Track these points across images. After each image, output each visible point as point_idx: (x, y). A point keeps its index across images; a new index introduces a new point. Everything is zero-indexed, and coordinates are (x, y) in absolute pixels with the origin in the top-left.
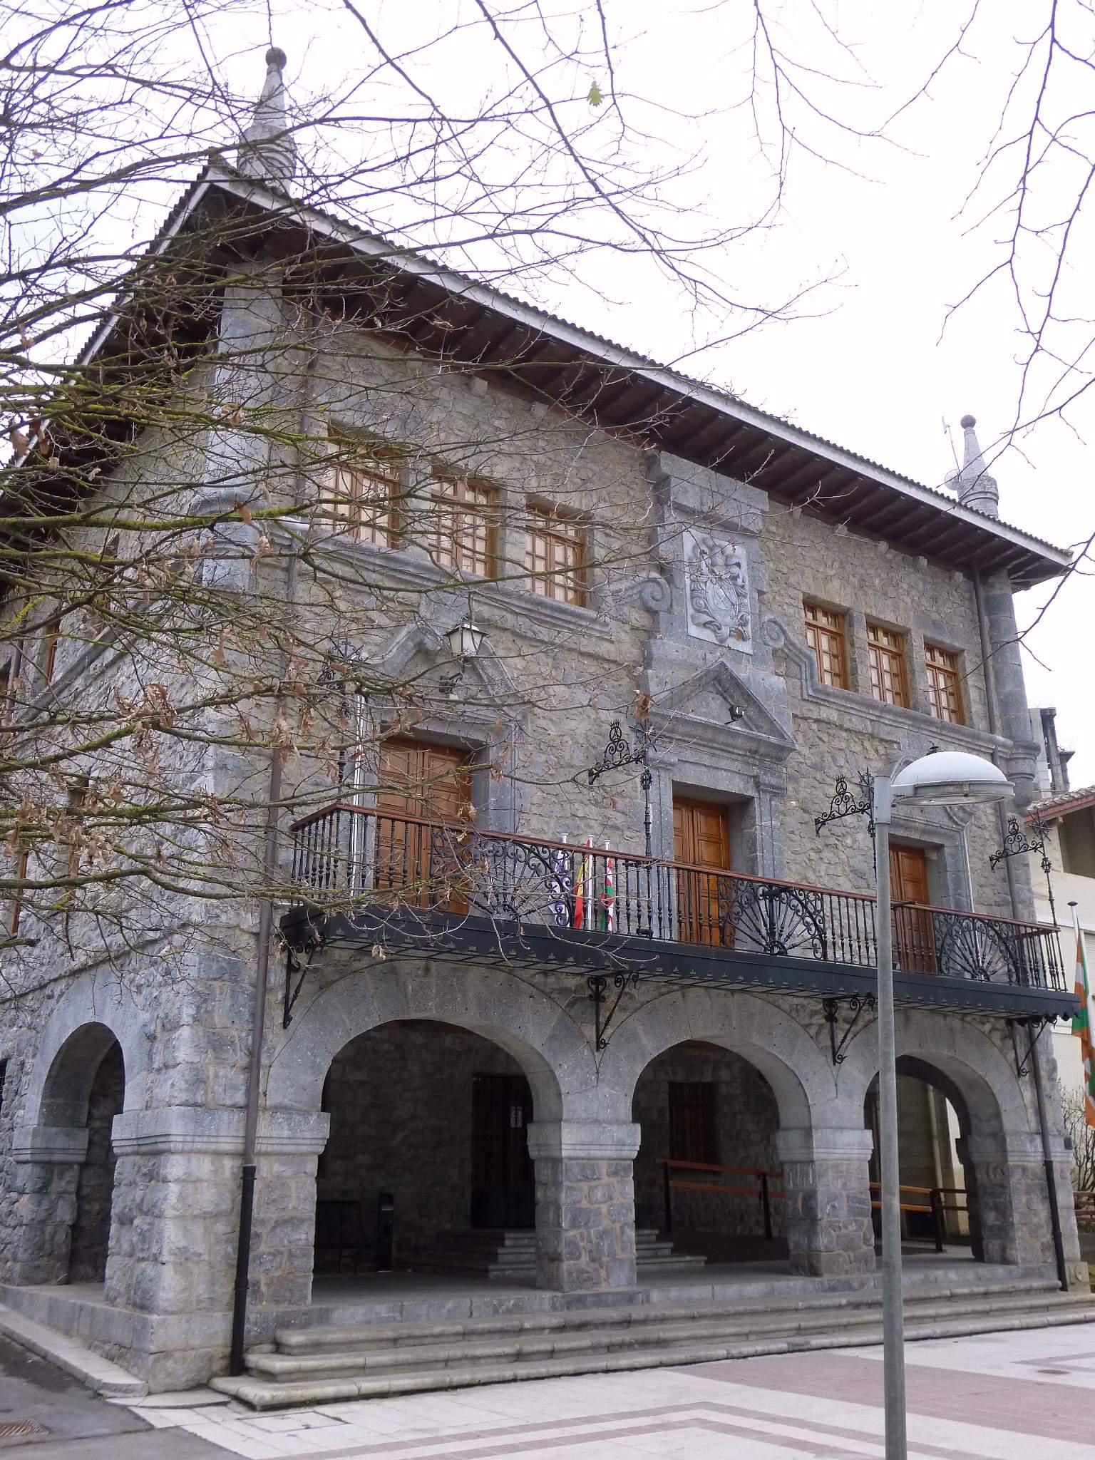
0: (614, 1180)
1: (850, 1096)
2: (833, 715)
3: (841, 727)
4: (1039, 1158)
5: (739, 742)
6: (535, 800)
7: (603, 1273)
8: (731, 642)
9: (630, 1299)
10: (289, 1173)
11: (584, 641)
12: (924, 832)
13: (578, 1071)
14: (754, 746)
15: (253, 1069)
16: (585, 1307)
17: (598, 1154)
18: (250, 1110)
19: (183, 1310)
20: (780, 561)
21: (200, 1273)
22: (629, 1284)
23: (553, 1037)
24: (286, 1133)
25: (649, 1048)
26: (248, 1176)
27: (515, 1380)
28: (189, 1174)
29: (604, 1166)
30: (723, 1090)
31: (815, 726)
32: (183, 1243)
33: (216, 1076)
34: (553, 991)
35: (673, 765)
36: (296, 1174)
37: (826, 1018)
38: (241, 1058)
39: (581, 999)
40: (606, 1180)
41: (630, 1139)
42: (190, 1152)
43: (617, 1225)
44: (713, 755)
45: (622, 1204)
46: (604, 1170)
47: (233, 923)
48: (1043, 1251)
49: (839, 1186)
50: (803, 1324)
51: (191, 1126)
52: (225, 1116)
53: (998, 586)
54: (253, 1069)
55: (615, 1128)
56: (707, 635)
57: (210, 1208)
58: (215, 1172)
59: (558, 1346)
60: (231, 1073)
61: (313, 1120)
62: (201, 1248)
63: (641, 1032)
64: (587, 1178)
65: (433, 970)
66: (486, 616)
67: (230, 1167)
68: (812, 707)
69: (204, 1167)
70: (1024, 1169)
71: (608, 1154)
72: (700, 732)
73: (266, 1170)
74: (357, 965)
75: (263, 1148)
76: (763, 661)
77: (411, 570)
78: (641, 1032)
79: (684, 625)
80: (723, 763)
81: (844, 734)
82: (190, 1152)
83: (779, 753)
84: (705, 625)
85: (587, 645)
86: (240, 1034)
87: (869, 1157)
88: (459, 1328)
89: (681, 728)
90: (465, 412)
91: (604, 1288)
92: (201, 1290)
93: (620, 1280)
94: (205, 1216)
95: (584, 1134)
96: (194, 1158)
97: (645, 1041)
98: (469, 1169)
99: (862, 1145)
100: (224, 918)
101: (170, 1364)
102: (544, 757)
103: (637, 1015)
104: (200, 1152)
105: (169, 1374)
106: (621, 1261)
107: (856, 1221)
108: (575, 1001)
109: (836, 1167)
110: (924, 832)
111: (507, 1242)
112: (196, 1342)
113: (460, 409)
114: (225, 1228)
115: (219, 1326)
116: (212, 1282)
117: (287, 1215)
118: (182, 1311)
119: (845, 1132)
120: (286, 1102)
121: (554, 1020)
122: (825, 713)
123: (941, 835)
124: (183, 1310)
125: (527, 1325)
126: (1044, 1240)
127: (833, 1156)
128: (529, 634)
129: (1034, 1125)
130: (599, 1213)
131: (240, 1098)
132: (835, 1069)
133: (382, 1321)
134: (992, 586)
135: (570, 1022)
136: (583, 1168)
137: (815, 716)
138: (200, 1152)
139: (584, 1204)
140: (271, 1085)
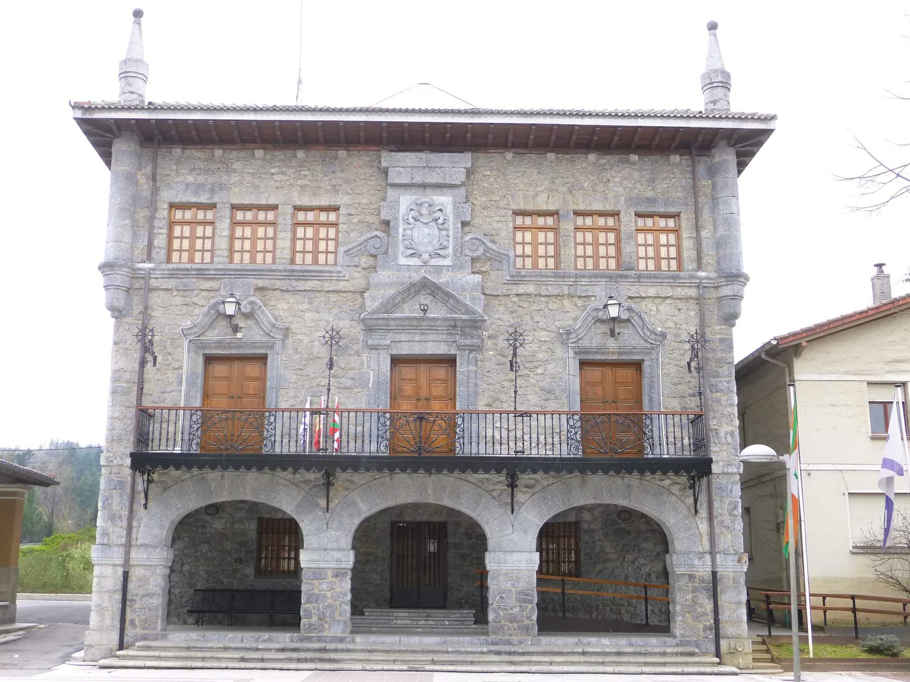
0: (335, 579)
1: (525, 532)
2: (531, 289)
3: (540, 295)
4: (709, 569)
5: (439, 323)
6: (292, 381)
7: (327, 626)
8: (433, 262)
9: (342, 640)
10: (148, 573)
11: (327, 284)
12: (620, 353)
13: (315, 523)
14: (452, 323)
15: (130, 528)
16: (311, 642)
17: (325, 566)
18: (128, 546)
19: (100, 629)
20: (492, 193)
21: (108, 615)
22: (343, 632)
23: (298, 506)
24: (145, 556)
25: (364, 509)
26: (126, 575)
27: (227, 668)
28: (101, 574)
29: (330, 573)
30: (585, 526)
31: (516, 299)
32: (99, 602)
33: (113, 532)
34: (300, 482)
35: (388, 346)
36: (152, 574)
37: (507, 485)
38: (125, 523)
39: (317, 485)
40: (330, 579)
41: (348, 559)
42: (102, 564)
43: (337, 603)
44: (423, 334)
45: (341, 592)
46: (329, 574)
47: (120, 463)
48: (704, 631)
49: (509, 585)
50: (435, 659)
51: (100, 554)
52: (116, 549)
53: (717, 155)
54: (130, 528)
55: (335, 553)
56: (415, 261)
57: (111, 588)
58: (114, 573)
59: (265, 657)
60: (120, 530)
61: (158, 550)
62: (107, 605)
63: (359, 501)
64: (316, 578)
65: (226, 478)
66: (260, 285)
67: (120, 570)
68: (511, 287)
69: (109, 571)
70: (691, 577)
71: (331, 566)
72: (407, 322)
73: (136, 574)
74: (183, 478)
75: (135, 563)
76: (461, 267)
77: (212, 272)
78: (359, 501)
79: (396, 259)
80: (430, 337)
81: (544, 299)
82: (102, 564)
83: (476, 324)
84: (412, 255)
85: (327, 286)
86: (125, 513)
87: (537, 569)
88: (221, 645)
89: (392, 323)
90: (251, 171)
91: (326, 633)
92: (108, 622)
93: (337, 630)
94: (110, 591)
95: (315, 556)
96: (104, 567)
97: (361, 505)
98: (387, 575)
99: (530, 561)
100: (115, 462)
101: (93, 650)
102: (298, 356)
103: (357, 492)
104: (106, 564)
105: (93, 655)
106: (338, 621)
107: (520, 606)
108: (314, 486)
109: (506, 574)
110: (620, 353)
111: (366, 614)
112: (104, 642)
113: (247, 170)
114: (118, 596)
115: (115, 636)
116: (113, 619)
117: (148, 592)
118: (100, 630)
119: (515, 554)
120: (148, 542)
121: (300, 497)
122: (521, 289)
123: (639, 353)
124: (100, 629)
125: (260, 647)
126: (707, 623)
127: (504, 568)
128: (290, 289)
129: (707, 547)
130: (325, 596)
131: (123, 541)
132: (512, 517)
133: (193, 640)
134: (714, 156)
135: (310, 498)
136: (314, 573)
137: (515, 292)
138: (106, 564)
139: (316, 591)
140: (140, 535)
